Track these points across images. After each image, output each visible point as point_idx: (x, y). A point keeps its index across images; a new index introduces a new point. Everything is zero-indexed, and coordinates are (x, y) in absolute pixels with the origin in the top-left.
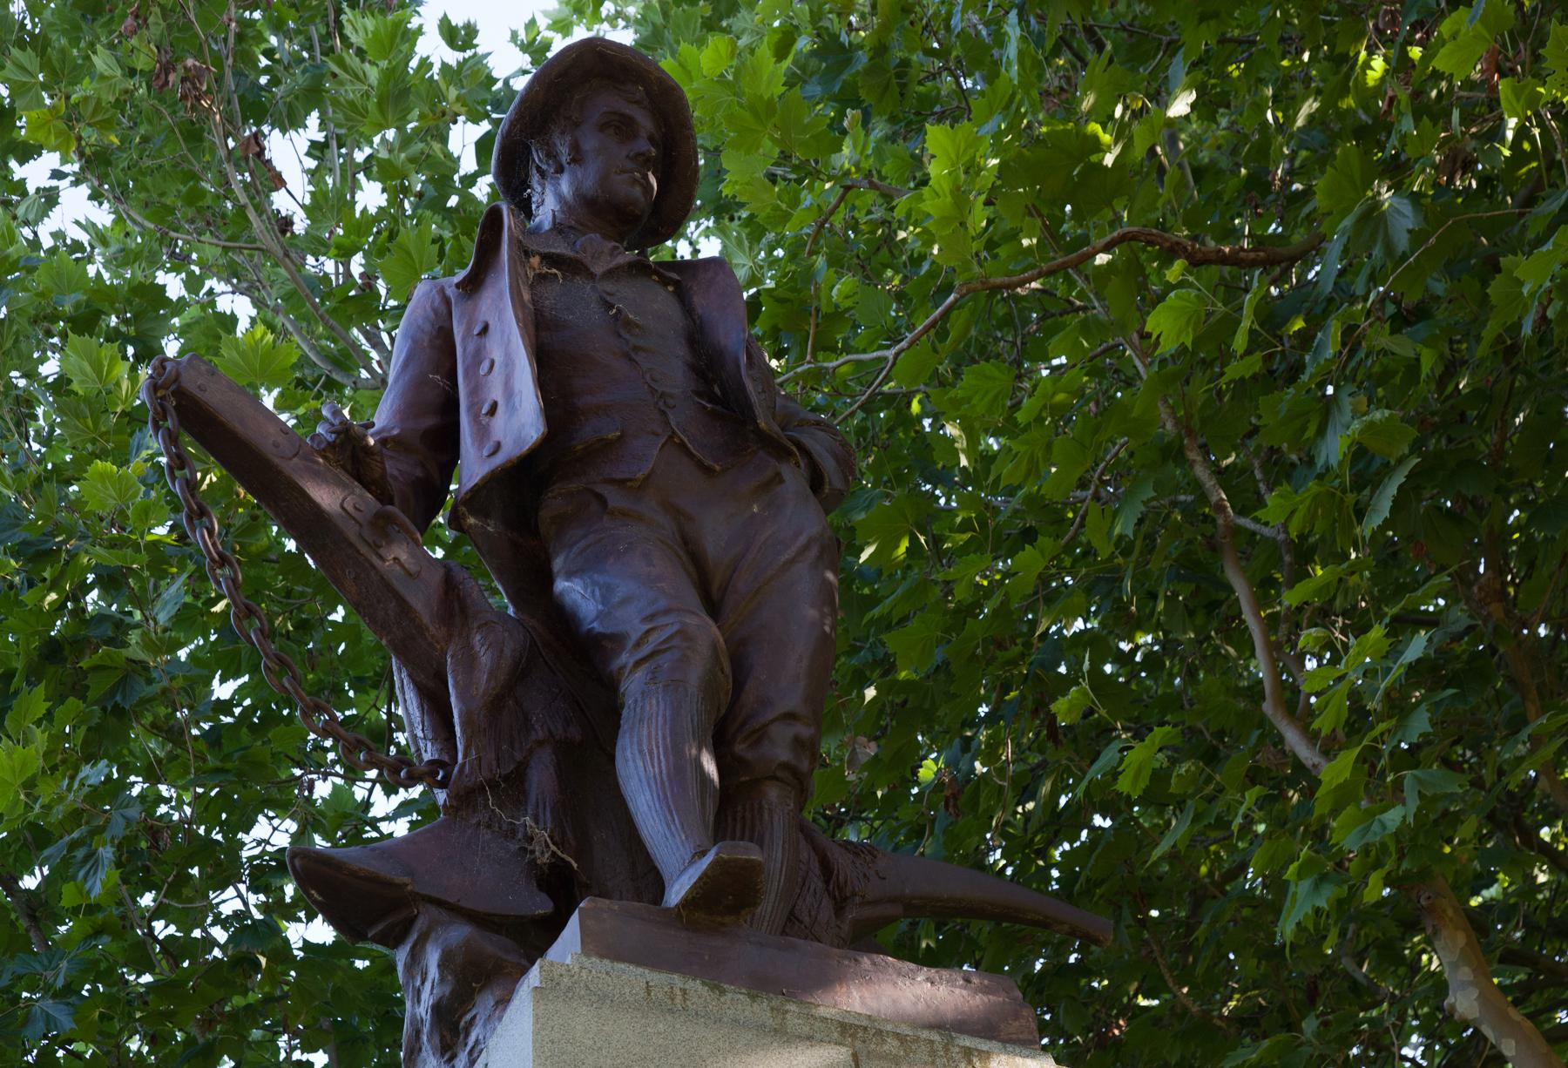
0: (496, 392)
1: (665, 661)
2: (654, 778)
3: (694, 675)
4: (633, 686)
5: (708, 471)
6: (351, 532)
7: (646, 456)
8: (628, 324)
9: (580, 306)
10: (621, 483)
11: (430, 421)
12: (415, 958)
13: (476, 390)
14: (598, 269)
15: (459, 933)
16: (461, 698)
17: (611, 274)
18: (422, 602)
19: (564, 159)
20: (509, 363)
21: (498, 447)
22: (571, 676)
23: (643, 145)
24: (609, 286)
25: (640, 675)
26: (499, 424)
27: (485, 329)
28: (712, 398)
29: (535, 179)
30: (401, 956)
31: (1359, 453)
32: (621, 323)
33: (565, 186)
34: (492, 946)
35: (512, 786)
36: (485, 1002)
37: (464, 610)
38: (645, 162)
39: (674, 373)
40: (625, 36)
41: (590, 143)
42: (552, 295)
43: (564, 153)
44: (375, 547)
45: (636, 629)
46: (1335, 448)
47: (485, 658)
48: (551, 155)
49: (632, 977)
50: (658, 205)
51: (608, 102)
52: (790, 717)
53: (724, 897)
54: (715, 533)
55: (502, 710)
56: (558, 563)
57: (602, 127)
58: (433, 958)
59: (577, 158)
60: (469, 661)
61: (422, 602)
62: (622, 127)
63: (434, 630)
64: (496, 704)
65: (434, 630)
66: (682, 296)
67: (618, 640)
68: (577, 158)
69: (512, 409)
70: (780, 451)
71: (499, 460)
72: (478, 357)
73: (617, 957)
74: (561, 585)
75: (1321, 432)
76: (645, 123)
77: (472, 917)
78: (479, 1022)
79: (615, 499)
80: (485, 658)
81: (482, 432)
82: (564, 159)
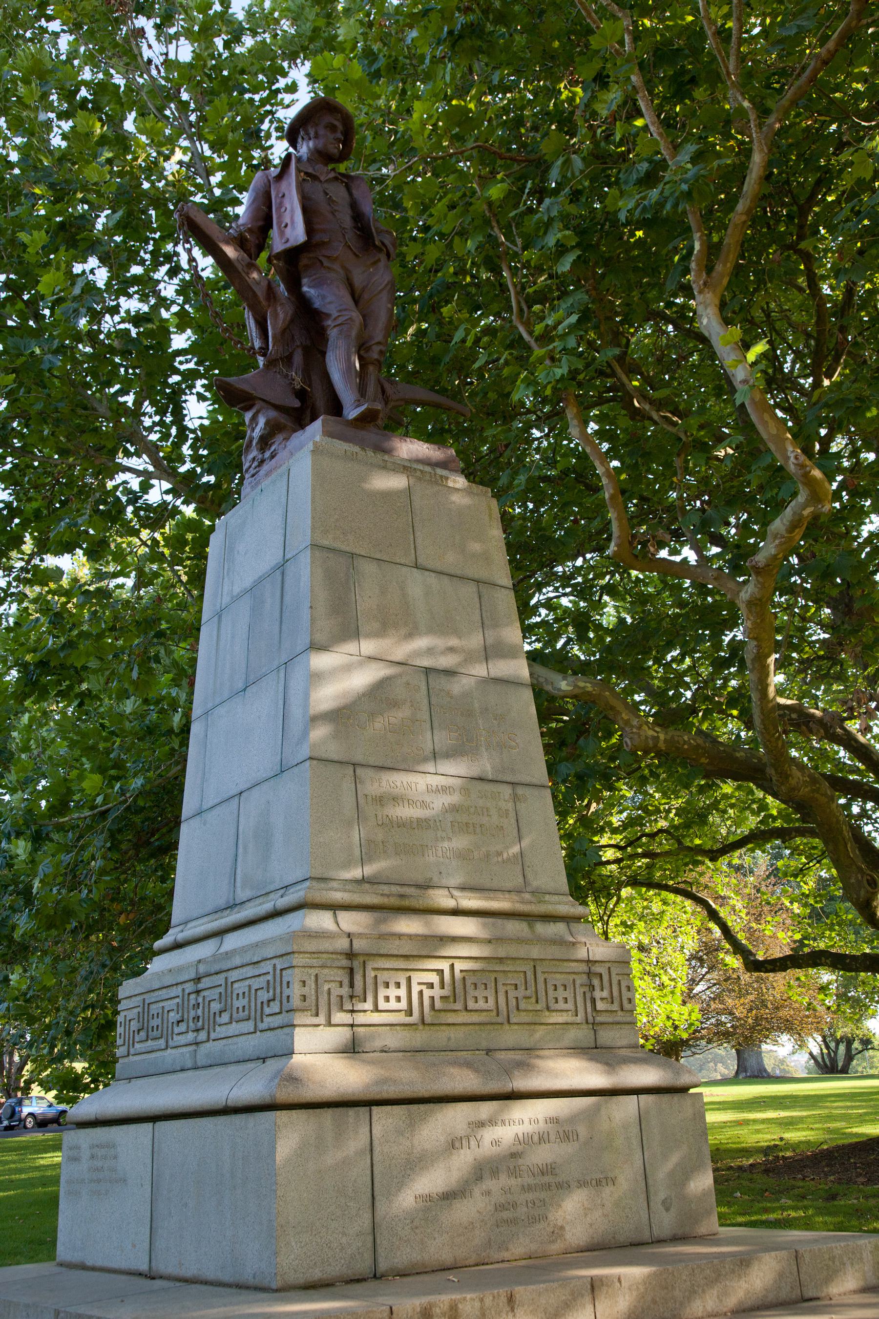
0: (287, 220)
1: (345, 327)
2: (340, 365)
3: (354, 333)
4: (333, 333)
5: (357, 256)
6: (240, 268)
7: (338, 249)
8: (334, 201)
9: (316, 191)
10: (329, 257)
11: (261, 223)
12: (254, 419)
13: (280, 217)
14: (322, 178)
15: (273, 414)
16: (273, 329)
17: (326, 181)
18: (261, 293)
19: (312, 135)
20: (292, 211)
21: (288, 241)
22: (310, 323)
23: (339, 135)
24: (326, 185)
25: (335, 330)
26: (288, 231)
27: (283, 196)
28: (359, 229)
29: (300, 140)
30: (248, 416)
31: (558, 244)
32: (330, 201)
33: (311, 144)
34: (283, 419)
35: (288, 360)
36: (279, 438)
37: (275, 297)
38: (339, 141)
39: (346, 219)
40: (459, 482)
41: (322, 132)
42: (307, 186)
43: (312, 134)
44: (248, 274)
45: (335, 314)
46: (551, 240)
47: (281, 316)
48: (308, 134)
49: (341, 446)
50: (341, 152)
51: (328, 119)
52: (379, 343)
53: (367, 419)
54: (358, 279)
55: (284, 335)
56: (305, 281)
57: (326, 127)
58: (262, 421)
59: (317, 136)
60: (275, 316)
61: (261, 293)
62: (333, 128)
63: (264, 303)
64: (284, 332)
65: (264, 303)
66: (348, 188)
67: (328, 316)
68: (317, 136)
69: (293, 228)
70: (380, 250)
71: (288, 245)
72: (280, 205)
73: (333, 437)
74: (305, 289)
75: (545, 233)
76: (340, 127)
77: (276, 407)
78: (277, 444)
79: (326, 263)
80: (281, 316)
81: (282, 233)
82: (312, 135)
